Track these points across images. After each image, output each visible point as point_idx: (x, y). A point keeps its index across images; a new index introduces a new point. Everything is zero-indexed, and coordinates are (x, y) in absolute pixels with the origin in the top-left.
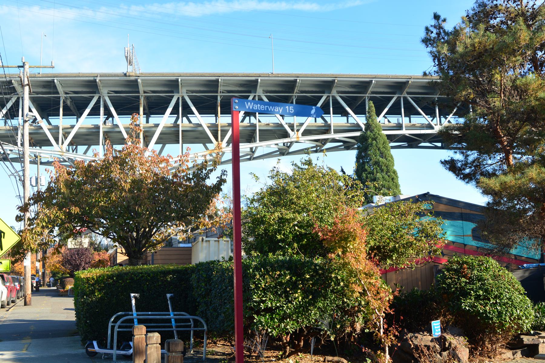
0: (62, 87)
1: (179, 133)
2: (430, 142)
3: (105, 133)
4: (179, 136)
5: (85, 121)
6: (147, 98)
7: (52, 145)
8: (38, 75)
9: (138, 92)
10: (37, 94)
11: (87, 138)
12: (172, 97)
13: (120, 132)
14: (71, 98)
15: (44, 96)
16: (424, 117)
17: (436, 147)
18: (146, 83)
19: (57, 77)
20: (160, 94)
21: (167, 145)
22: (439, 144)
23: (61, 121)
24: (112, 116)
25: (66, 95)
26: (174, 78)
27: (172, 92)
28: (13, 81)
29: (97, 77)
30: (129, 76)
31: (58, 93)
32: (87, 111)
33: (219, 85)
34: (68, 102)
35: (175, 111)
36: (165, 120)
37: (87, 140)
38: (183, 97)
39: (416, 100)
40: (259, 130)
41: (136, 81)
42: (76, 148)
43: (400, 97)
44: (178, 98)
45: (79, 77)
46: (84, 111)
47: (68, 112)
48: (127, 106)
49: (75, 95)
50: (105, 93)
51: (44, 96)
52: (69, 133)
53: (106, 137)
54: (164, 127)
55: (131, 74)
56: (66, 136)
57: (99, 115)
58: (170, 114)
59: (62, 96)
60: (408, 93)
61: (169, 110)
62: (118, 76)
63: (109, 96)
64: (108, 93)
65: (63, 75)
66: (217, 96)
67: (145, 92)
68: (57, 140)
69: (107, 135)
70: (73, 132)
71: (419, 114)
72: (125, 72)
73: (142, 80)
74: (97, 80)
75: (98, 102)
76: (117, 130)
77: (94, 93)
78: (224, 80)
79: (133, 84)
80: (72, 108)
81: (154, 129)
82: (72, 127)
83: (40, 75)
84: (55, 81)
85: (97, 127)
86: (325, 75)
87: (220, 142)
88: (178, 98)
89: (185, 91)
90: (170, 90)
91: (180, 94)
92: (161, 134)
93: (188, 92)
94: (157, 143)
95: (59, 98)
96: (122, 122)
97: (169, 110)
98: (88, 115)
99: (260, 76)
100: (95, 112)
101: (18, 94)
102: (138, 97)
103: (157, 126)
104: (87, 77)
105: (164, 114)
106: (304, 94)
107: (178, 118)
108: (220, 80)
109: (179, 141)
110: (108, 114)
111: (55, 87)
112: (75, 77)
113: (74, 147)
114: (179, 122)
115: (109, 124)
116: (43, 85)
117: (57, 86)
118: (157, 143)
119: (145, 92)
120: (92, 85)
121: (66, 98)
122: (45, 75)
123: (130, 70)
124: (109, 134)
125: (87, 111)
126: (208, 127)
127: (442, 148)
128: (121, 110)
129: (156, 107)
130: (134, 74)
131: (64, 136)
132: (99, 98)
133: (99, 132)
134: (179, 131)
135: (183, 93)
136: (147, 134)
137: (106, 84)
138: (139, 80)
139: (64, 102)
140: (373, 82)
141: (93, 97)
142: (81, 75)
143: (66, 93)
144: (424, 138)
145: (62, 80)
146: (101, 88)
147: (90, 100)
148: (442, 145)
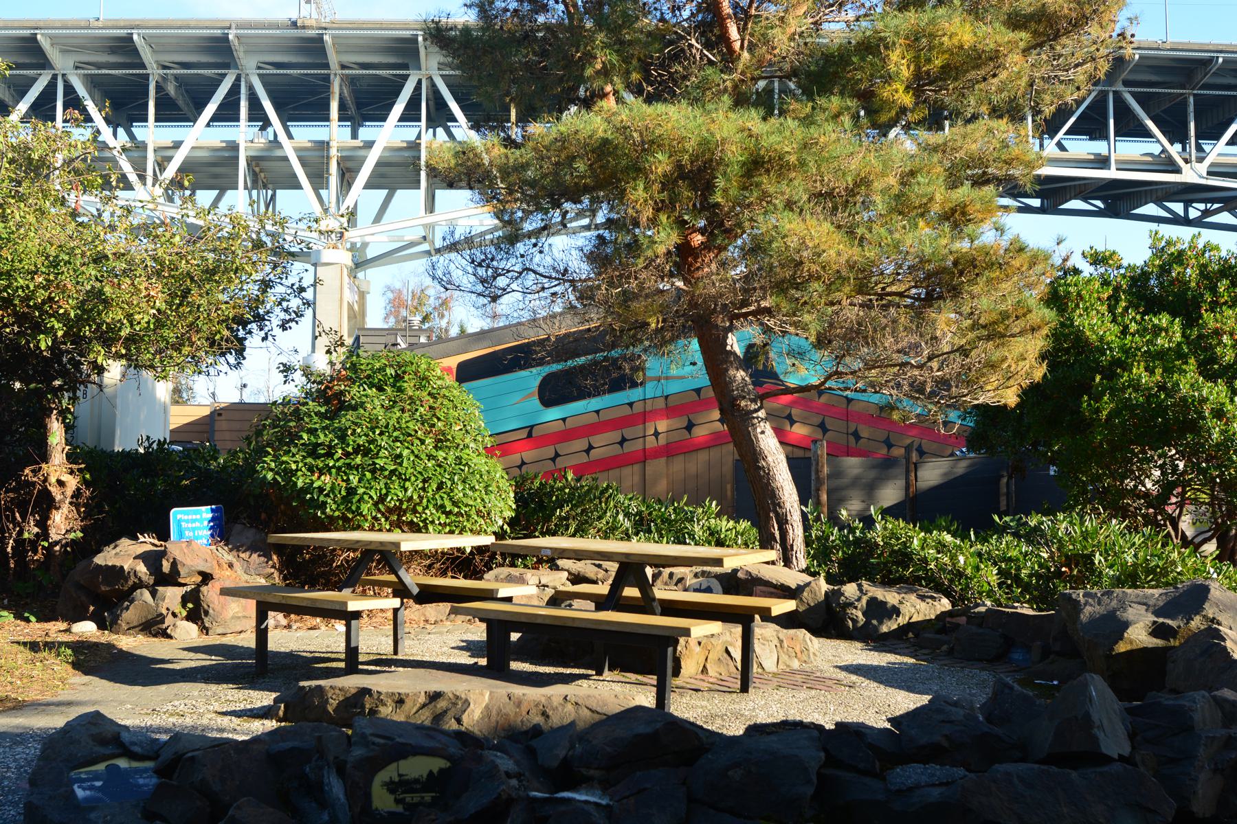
0: (154, 51)
2: (1085, 200)
3: (251, 161)
5: (200, 135)
6: (352, 81)
7: (298, 186)
8: (96, 24)
9: (327, 66)
10: (99, 68)
11: (213, 171)
12: (406, 77)
13: (286, 159)
14: (176, 77)
15: (113, 72)
16: (1158, 141)
17: (1027, 209)
18: (344, 45)
19: (138, 27)
20: (289, 72)
21: (399, 191)
22: (1036, 203)
23: (152, 133)
25: (161, 72)
27: (406, 67)
28: (39, 37)
29: (229, 28)
30: (304, 27)
31: (143, 66)
32: (211, 109)
34: (171, 89)
35: (410, 115)
36: (389, 134)
37: (216, 176)
38: (430, 79)
39: (1142, 99)
41: (320, 39)
42: (273, 196)
43: (1107, 92)
44: (419, 82)
45: (189, 28)
47: (170, 112)
48: (301, 101)
51: (113, 72)
52: (169, 159)
54: (385, 148)
55: (307, 23)
56: (161, 165)
57: (238, 120)
58: (400, 120)
59: (154, 73)
60: (1126, 83)
61: (398, 108)
62: (278, 28)
64: (259, 68)
65: (179, 24)
67: (343, 67)
68: (142, 178)
69: (257, 165)
70: (179, 158)
71: (1147, 134)
72: (294, 17)
73: (334, 37)
74: (231, 37)
75: (234, 91)
76: (278, 153)
77: (227, 66)
79: (313, 47)
80: (180, 103)
81: (362, 153)
82: (177, 145)
83: (100, 24)
84: (135, 37)
85: (233, 147)
88: (419, 82)
89: (436, 66)
90: (399, 61)
91: (423, 72)
92: (378, 164)
94: (369, 186)
95: (146, 77)
97: (398, 108)
98: (401, 119)
100: (227, 113)
102: (327, 78)
103: (369, 145)
104: (207, 28)
105: (384, 120)
106: (107, 72)
109: (419, 181)
110: (257, 114)
111: (135, 51)
112: (180, 28)
113: (270, 192)
115: (261, 141)
116: (110, 47)
117: (140, 49)
118: (369, 186)
119: (343, 67)
120: (219, 49)
121: (165, 78)
122: (110, 24)
125: (211, 109)
127: (1041, 210)
128: (294, 109)
129: (368, 103)
131: (159, 165)
132: (238, 79)
133: (237, 158)
136: (349, 164)
137: (254, 46)
138: (326, 38)
139: (159, 88)
140: (1220, 60)
141: (224, 75)
142: (193, 24)
143: (165, 67)
144: (1085, 189)
145: (151, 36)
146: (241, 55)
147: (215, 84)
148: (1042, 203)
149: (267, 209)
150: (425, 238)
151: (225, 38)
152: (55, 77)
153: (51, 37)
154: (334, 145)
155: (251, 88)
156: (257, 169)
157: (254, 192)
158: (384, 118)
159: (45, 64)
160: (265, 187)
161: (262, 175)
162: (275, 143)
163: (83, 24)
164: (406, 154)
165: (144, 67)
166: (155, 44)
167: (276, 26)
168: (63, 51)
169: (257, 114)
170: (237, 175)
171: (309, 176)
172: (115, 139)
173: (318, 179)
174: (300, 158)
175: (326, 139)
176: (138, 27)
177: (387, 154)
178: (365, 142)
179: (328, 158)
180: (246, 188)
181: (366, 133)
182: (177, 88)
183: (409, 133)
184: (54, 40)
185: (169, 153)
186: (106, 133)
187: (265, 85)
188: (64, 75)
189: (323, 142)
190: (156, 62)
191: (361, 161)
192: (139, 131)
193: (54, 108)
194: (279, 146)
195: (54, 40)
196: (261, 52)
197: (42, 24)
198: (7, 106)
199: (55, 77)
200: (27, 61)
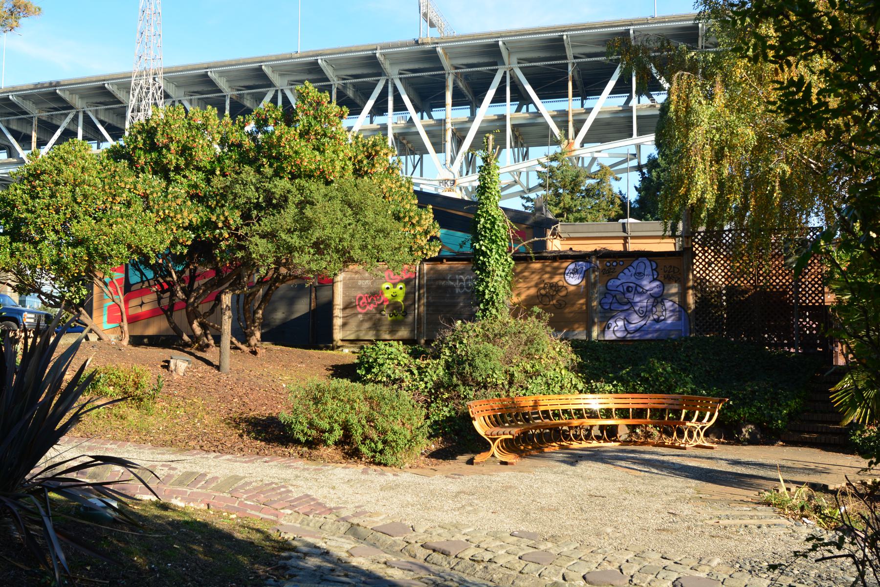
1: (632, 122)
4: (632, 126)
8: (296, 55)
13: (418, 133)
14: (354, 85)
18: (578, 42)
19: (321, 55)
20: (598, 59)
24: (530, 101)
25: (341, 82)
26: (691, 23)
27: (495, 64)
30: (423, 44)
32: (611, 84)
33: (566, 45)
35: (499, 98)
36: (605, 103)
40: (638, 117)
44: (505, 73)
46: (485, 95)
49: (589, 59)
50: (393, 71)
51: (537, 64)
52: (583, 122)
53: (517, 134)
54: (483, 121)
58: (492, 102)
63: (520, 68)
64: (400, 74)
65: (181, 69)
66: (567, 64)
67: (575, 57)
72: (417, 38)
73: (444, 49)
75: (385, 88)
76: (413, 130)
78: (571, 36)
79: (431, 56)
81: (467, 125)
84: (319, 61)
86: (466, 36)
87: (571, 141)
88: (505, 73)
89: (515, 61)
90: (491, 60)
91: (507, 66)
93: (520, 61)
96: (547, 109)
97: (491, 93)
98: (612, 93)
99: (632, 25)
100: (499, 98)
101: (274, 86)
102: (443, 77)
103: (589, 111)
104: (362, 51)
106: (596, 59)
107: (630, 98)
108: (565, 37)
110: (399, 106)
112: (346, 52)
113: (417, 157)
114: (634, 103)
121: (345, 86)
122: (304, 54)
123: (428, 35)
124: (522, 129)
126: (553, 117)
128: (434, 99)
130: (429, 41)
134: (631, 117)
135: (512, 66)
137: (395, 60)
138: (439, 50)
142: (353, 49)
143: (456, 68)
145: (331, 60)
147: (373, 86)
149: (415, 167)
150: (516, 182)
151: (374, 57)
152: (277, 91)
153: (272, 66)
154: (449, 121)
155: (395, 89)
156: (405, 142)
157: (516, 149)
158: (599, 93)
159: (270, 84)
160: (522, 146)
161: (410, 145)
162: (538, 114)
163: (288, 56)
164: (622, 115)
165: (328, 80)
166: (335, 64)
167: (402, 45)
168: (281, 75)
169: (399, 106)
170: (505, 140)
171: (433, 144)
172: (420, 123)
173: (439, 147)
174: (428, 132)
175: (443, 117)
176: (321, 55)
177: (485, 125)
178: (586, 109)
179: (445, 130)
180: (511, 147)
181: (588, 103)
182: (355, 92)
183: (620, 101)
184: (274, 68)
185: (582, 117)
186: (416, 117)
187: (525, 75)
188: (282, 90)
189: (441, 120)
190: (337, 76)
191: (467, 130)
192: (437, 114)
193: (387, 101)
194: (540, 115)
195: (274, 68)
196: (401, 63)
197: (264, 59)
198: (359, 106)
199: (277, 91)
200: (107, 100)
